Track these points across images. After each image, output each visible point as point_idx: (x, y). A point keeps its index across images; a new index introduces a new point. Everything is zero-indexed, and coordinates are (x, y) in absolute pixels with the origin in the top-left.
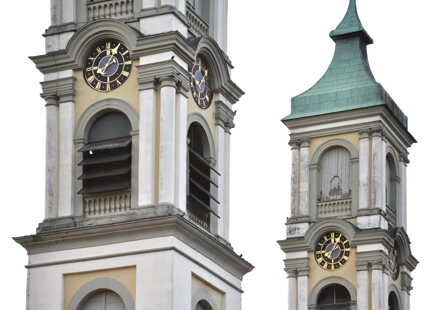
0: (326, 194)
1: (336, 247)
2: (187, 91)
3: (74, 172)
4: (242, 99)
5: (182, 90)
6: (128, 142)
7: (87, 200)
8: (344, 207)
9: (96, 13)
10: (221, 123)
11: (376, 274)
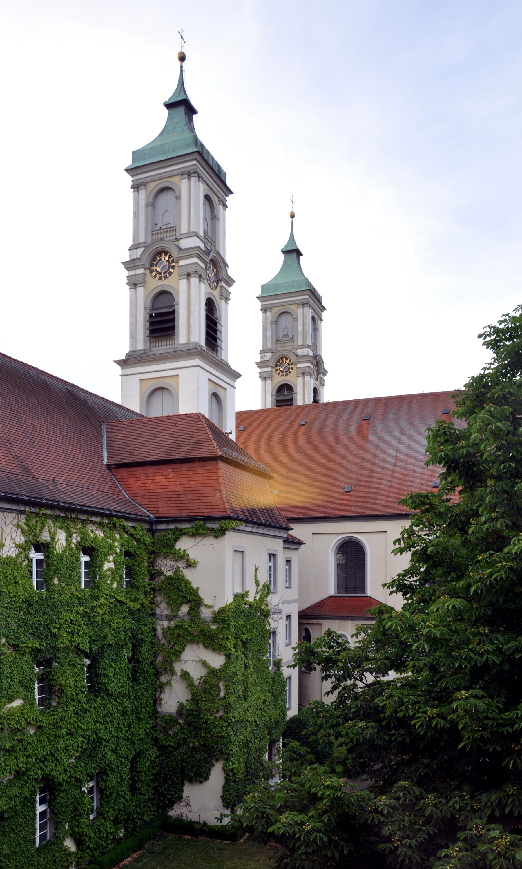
0: (281, 337)
1: (286, 365)
2: (205, 280)
3: (145, 326)
4: (234, 284)
5: (202, 279)
6: (173, 309)
7: (152, 341)
8: (290, 344)
9: (157, 237)
10: (223, 298)
11: (307, 378)
